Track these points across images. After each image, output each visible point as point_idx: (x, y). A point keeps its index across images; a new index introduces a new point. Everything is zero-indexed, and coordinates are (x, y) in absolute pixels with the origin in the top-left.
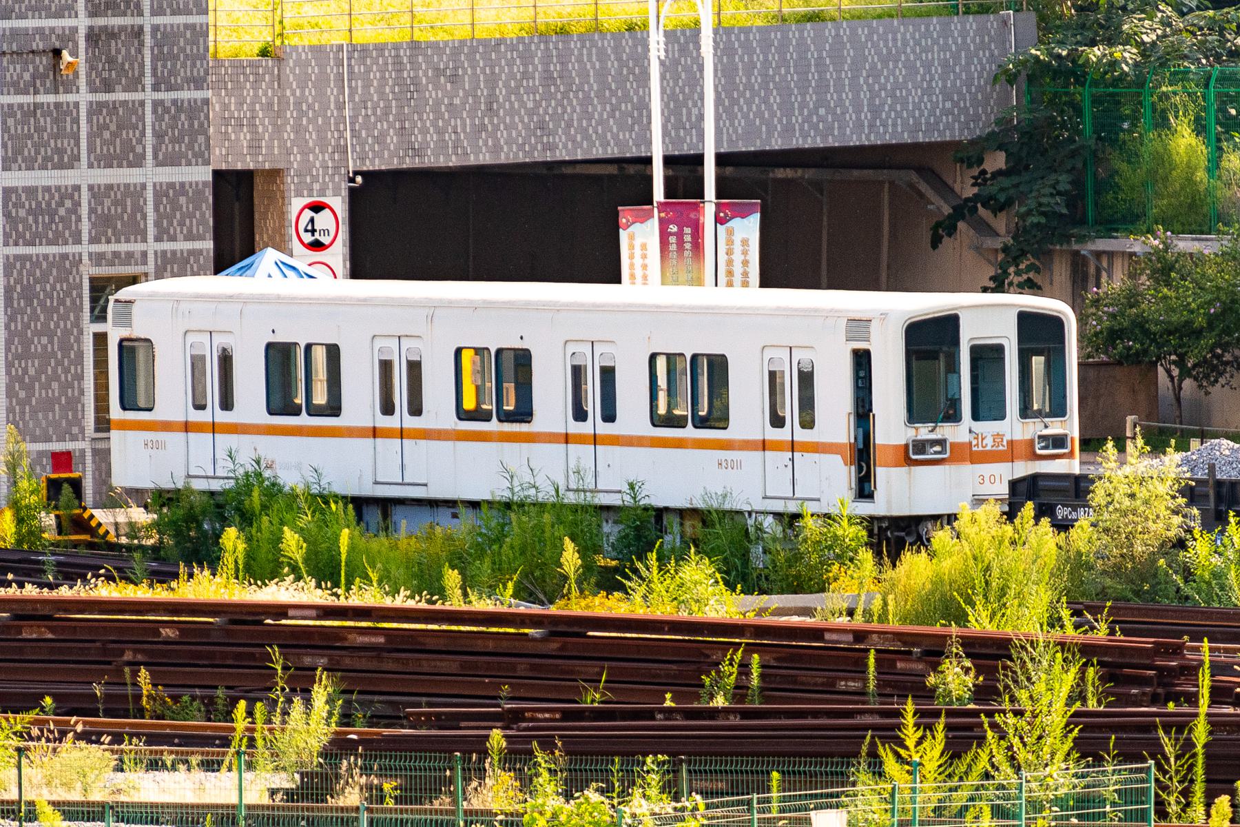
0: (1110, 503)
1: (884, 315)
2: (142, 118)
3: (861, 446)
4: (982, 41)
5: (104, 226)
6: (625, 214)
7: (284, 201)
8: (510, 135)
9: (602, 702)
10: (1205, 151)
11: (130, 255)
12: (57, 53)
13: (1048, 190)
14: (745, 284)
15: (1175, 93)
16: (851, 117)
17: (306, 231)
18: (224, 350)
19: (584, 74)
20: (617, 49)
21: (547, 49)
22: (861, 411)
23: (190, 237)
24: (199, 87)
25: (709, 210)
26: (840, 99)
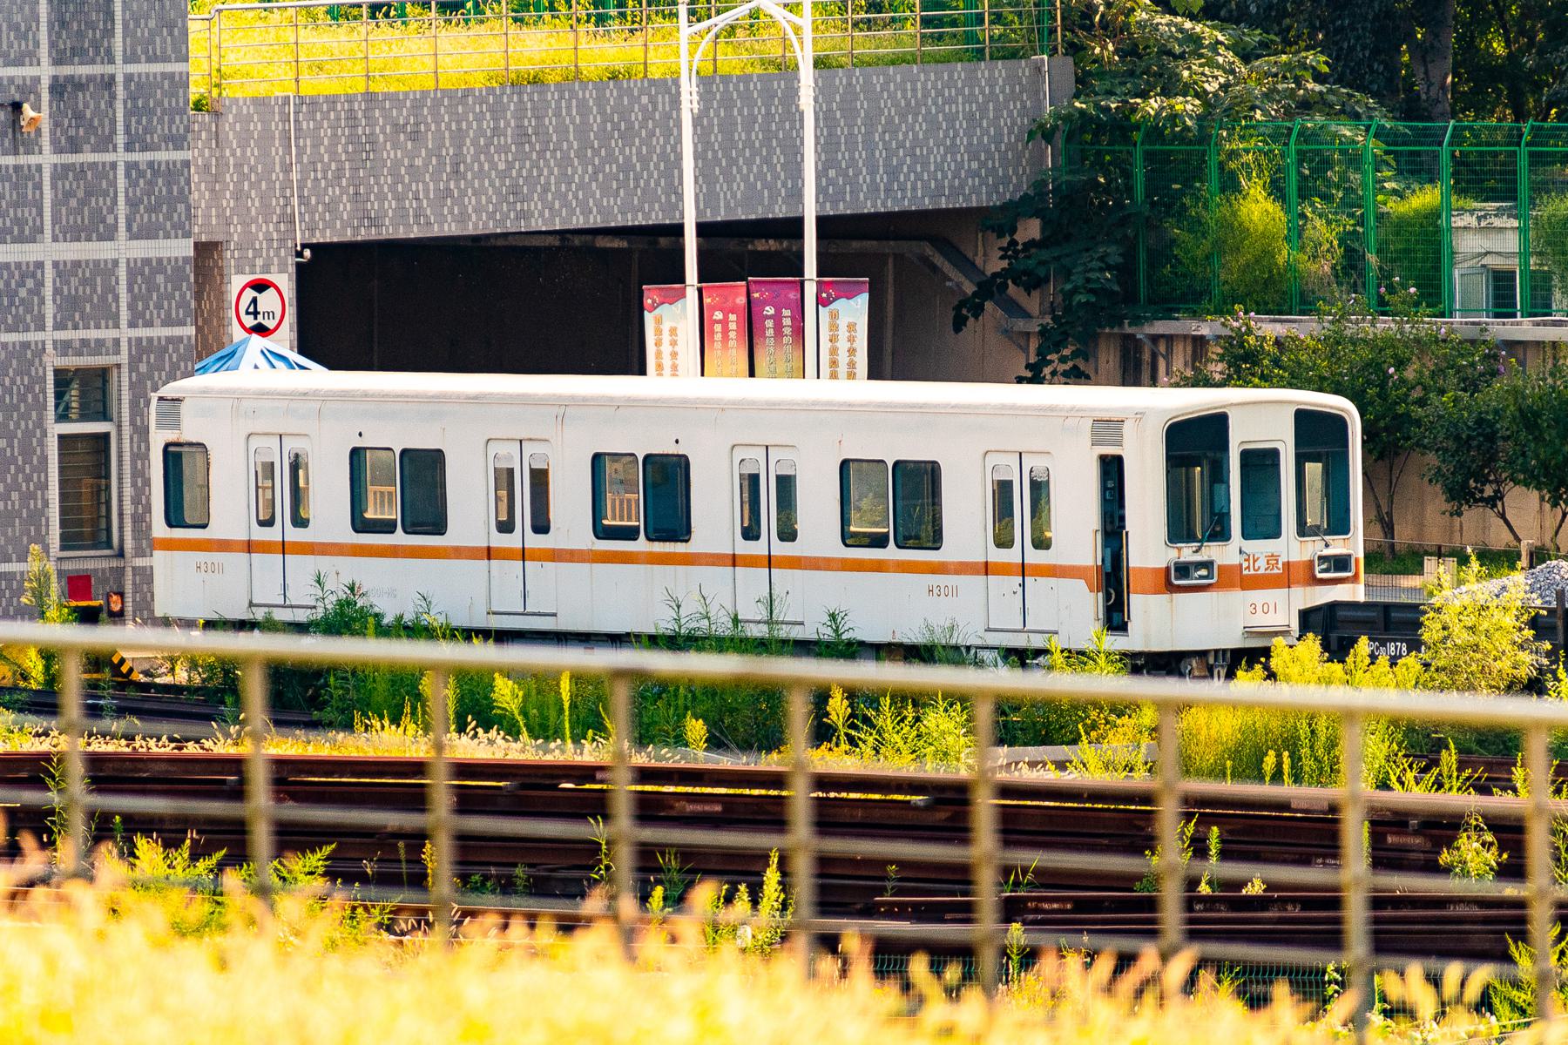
0: (1446, 638)
1: (1140, 415)
2: (114, 184)
3: (1109, 569)
4: (1013, 91)
5: (71, 312)
6: (651, 294)
7: (223, 279)
8: (479, 202)
9: (900, 880)
10: (1284, 219)
11: (100, 343)
12: (17, 107)
13: (1095, 264)
14: (852, 376)
15: (1247, 151)
16: (864, 178)
17: (248, 313)
18: (297, 456)
19: (562, 130)
20: (601, 101)
21: (521, 101)
22: (1109, 528)
23: (168, 322)
24: (178, 147)
25: (811, 290)
26: (852, 158)
